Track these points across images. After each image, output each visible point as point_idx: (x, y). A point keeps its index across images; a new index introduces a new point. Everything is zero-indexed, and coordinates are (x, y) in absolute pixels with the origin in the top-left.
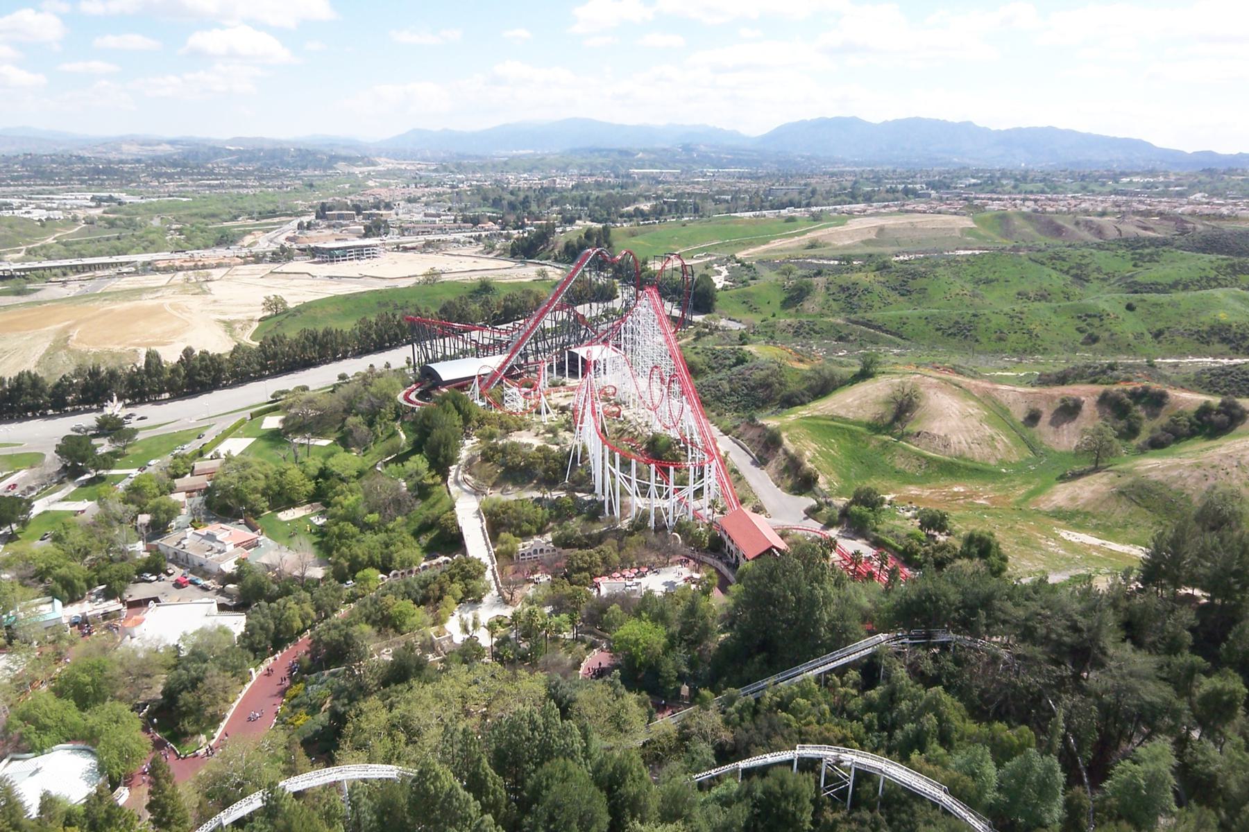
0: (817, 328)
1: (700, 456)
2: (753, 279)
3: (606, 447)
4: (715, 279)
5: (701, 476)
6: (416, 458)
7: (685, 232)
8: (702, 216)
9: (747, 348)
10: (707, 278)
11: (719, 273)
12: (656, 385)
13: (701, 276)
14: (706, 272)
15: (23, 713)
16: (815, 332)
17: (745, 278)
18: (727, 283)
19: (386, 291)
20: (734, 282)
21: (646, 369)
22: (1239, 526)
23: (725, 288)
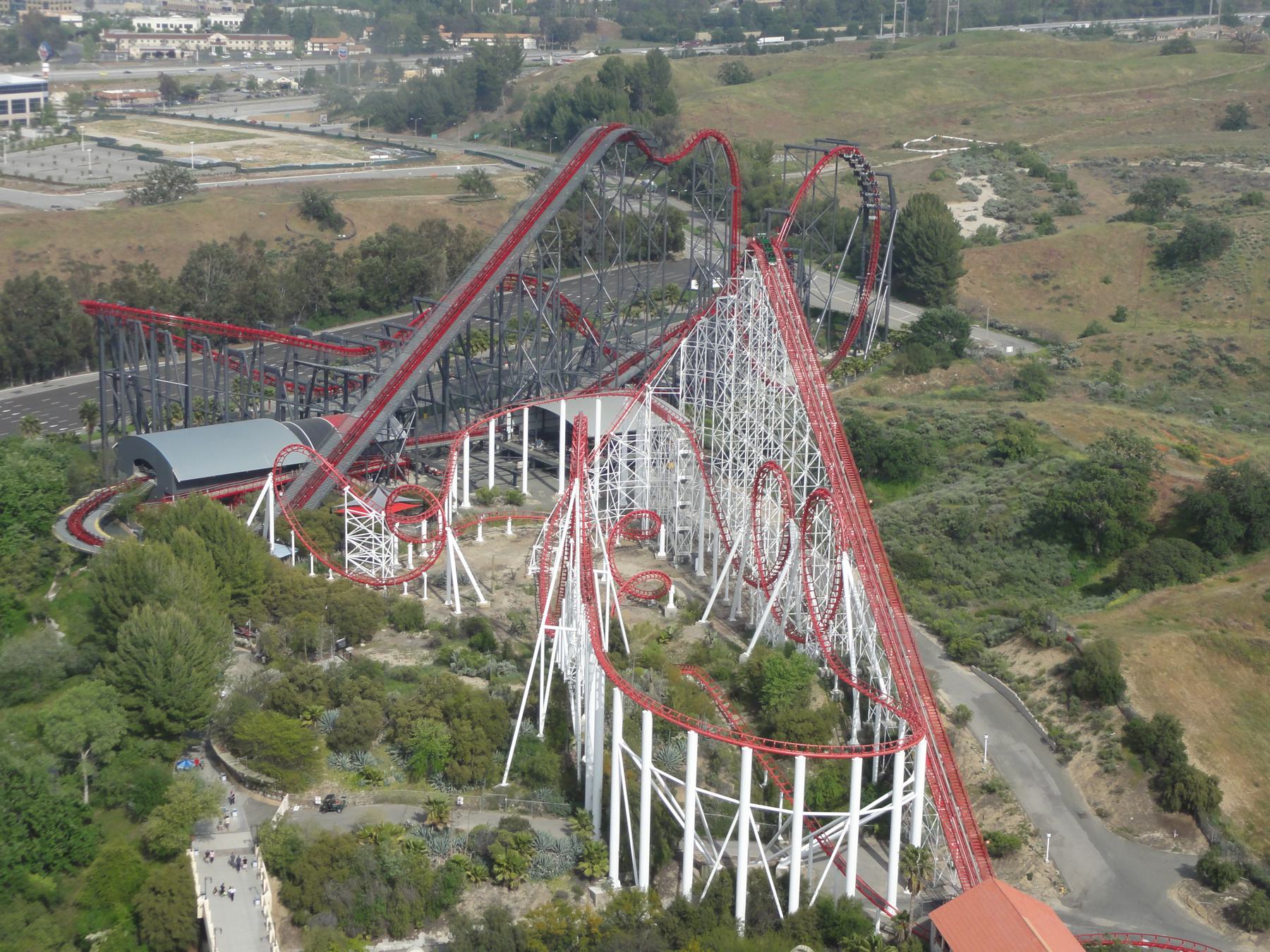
0: (1238, 358)
1: (890, 723)
2: (1067, 211)
3: (618, 694)
4: (959, 210)
5: (886, 783)
6: (88, 688)
7: (880, 71)
8: (930, 30)
9: (1034, 411)
10: (934, 203)
11: (969, 194)
12: (772, 512)
13: (916, 199)
14: (933, 189)
15: (425, 290)
16: (1237, 370)
17: (1045, 209)
18: (992, 222)
19: (345, 181)
20: (1009, 219)
21: (745, 468)
22: (984, 310)
23: (985, 238)
